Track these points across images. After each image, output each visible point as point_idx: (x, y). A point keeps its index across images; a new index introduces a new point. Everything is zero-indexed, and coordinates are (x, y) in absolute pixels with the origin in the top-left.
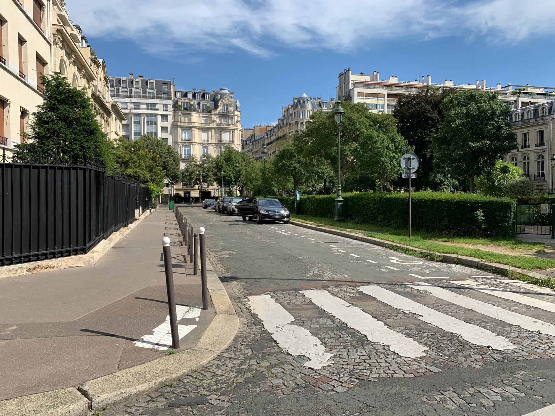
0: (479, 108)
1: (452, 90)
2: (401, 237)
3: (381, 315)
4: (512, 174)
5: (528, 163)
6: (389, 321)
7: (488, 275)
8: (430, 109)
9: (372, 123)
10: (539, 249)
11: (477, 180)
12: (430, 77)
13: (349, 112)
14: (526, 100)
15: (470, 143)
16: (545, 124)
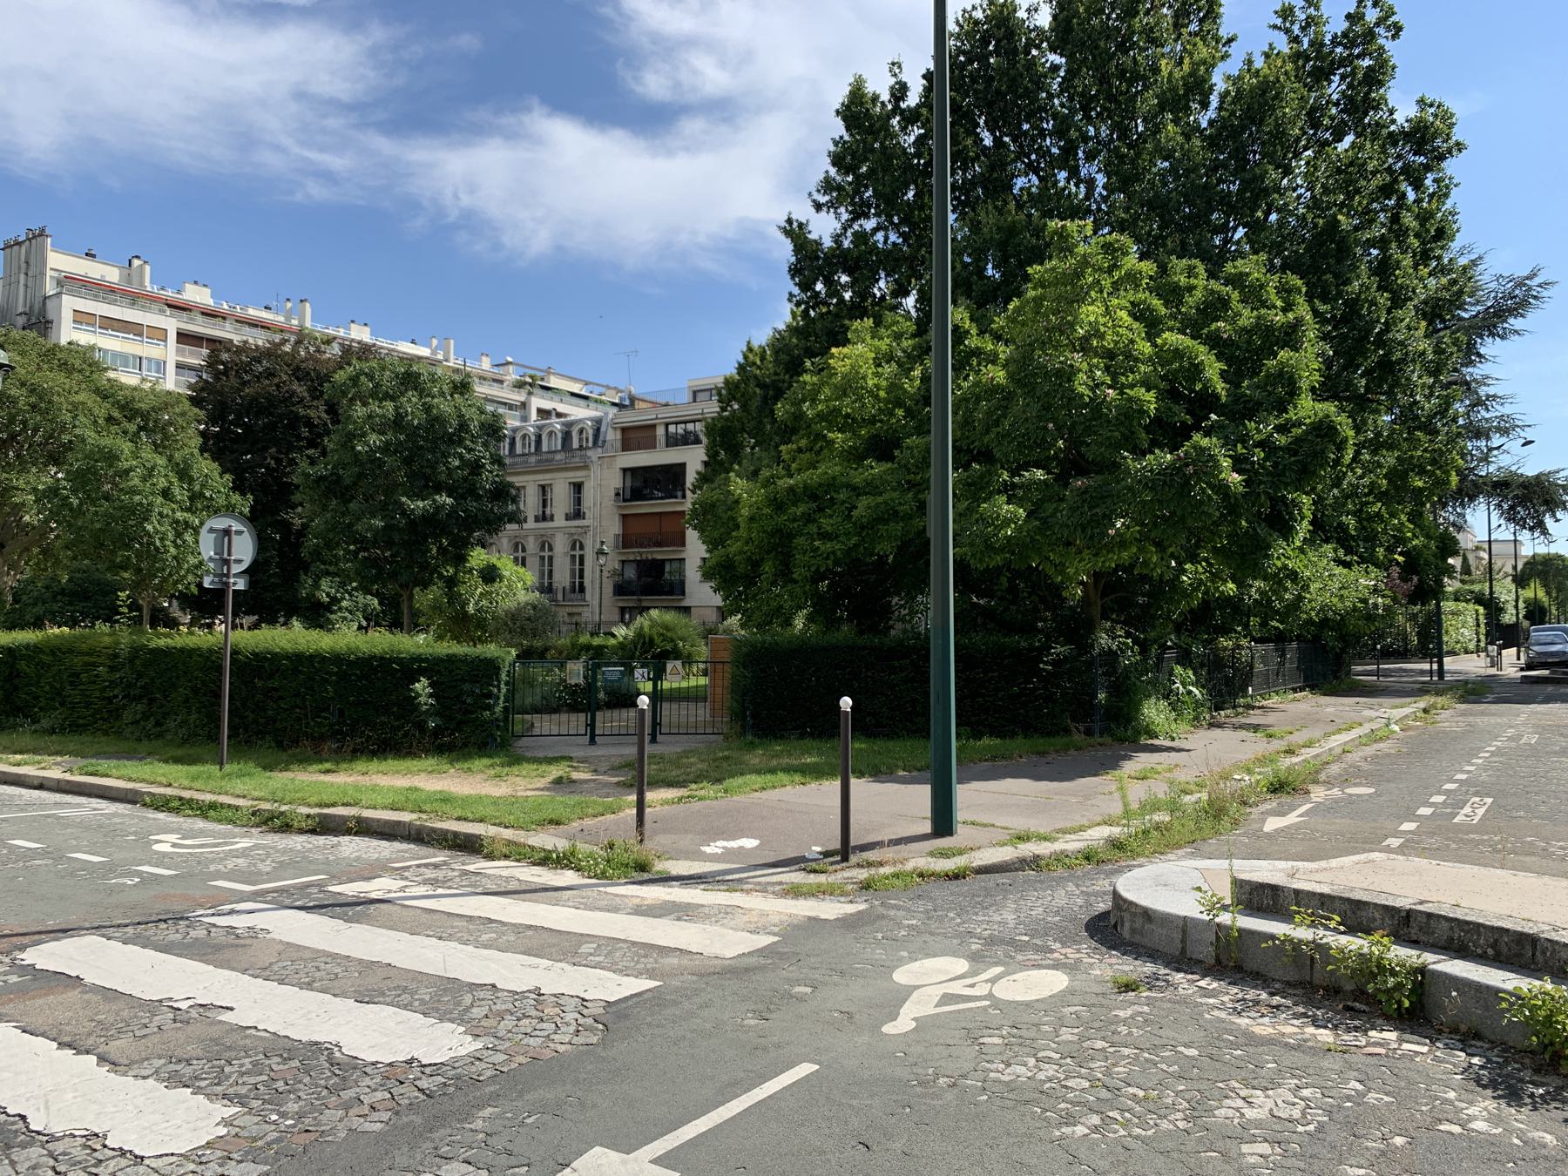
0: (428, 409)
1: (366, 351)
2: (194, 769)
3: (89, 1034)
4: (509, 587)
5: (551, 558)
6: (114, 1048)
7: (435, 856)
8: (306, 394)
9: (116, 414)
10: (560, 773)
11: (426, 597)
12: (308, 305)
13: (33, 368)
14: (547, 405)
15: (404, 499)
16: (586, 467)
